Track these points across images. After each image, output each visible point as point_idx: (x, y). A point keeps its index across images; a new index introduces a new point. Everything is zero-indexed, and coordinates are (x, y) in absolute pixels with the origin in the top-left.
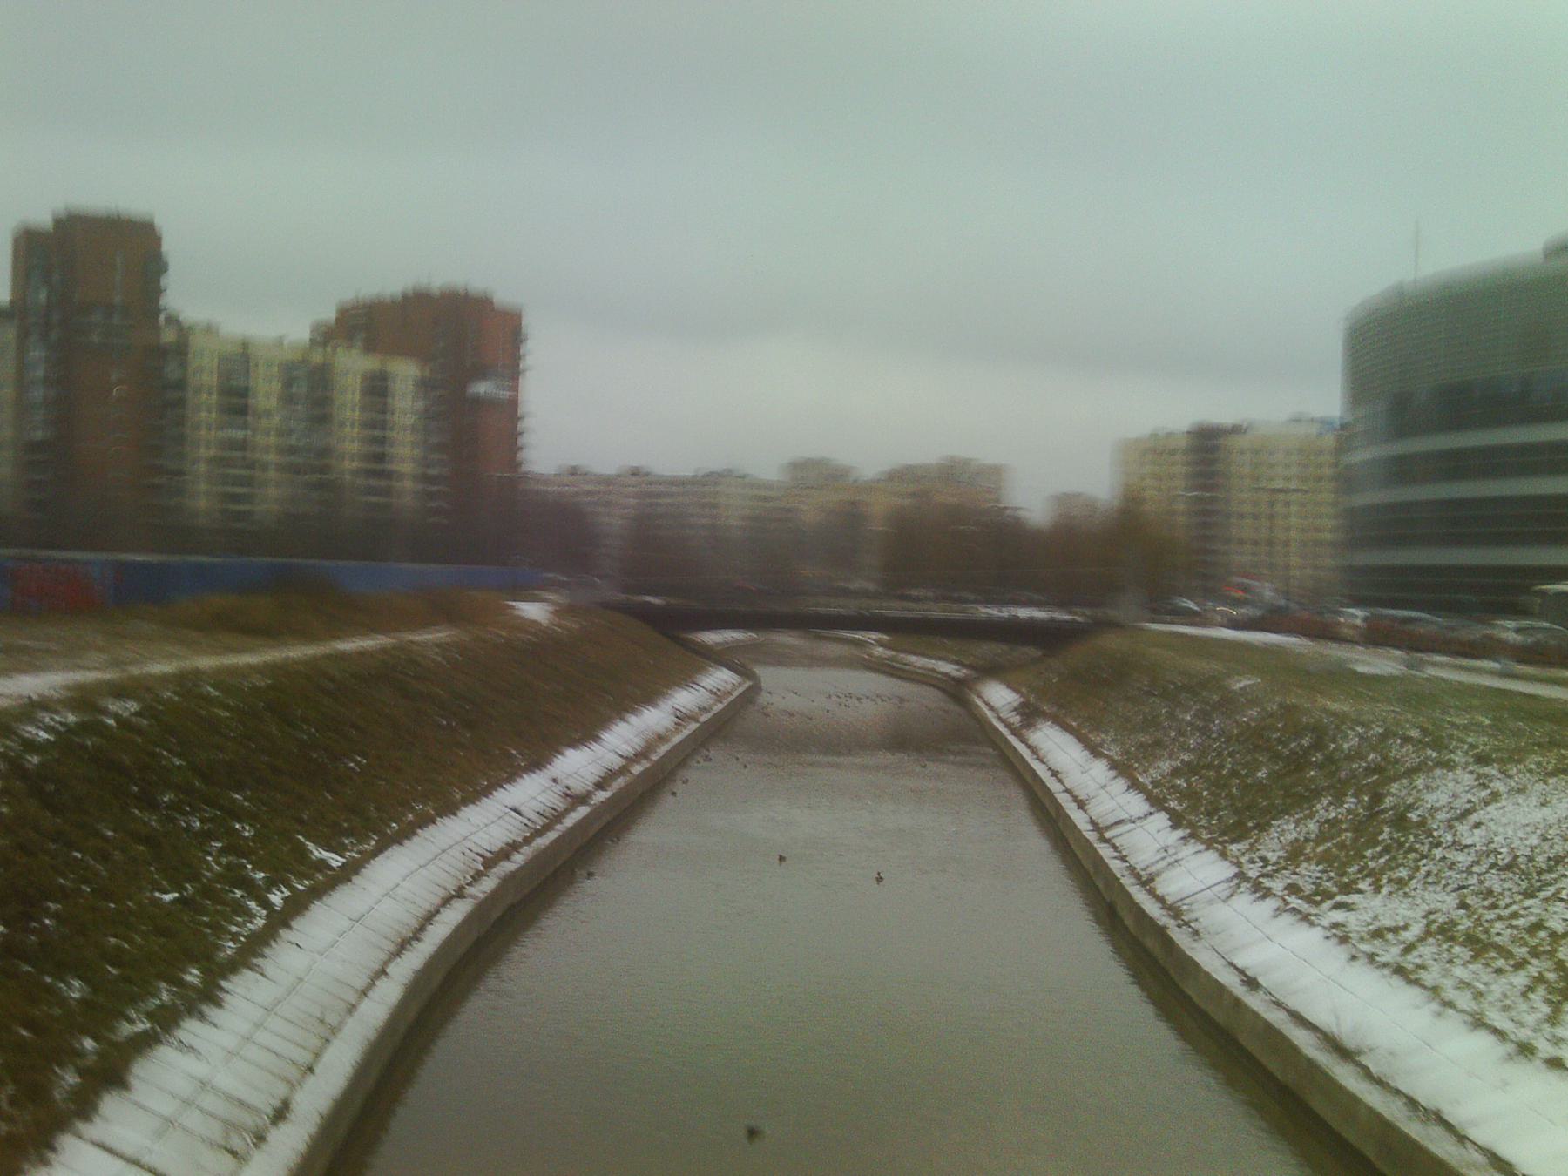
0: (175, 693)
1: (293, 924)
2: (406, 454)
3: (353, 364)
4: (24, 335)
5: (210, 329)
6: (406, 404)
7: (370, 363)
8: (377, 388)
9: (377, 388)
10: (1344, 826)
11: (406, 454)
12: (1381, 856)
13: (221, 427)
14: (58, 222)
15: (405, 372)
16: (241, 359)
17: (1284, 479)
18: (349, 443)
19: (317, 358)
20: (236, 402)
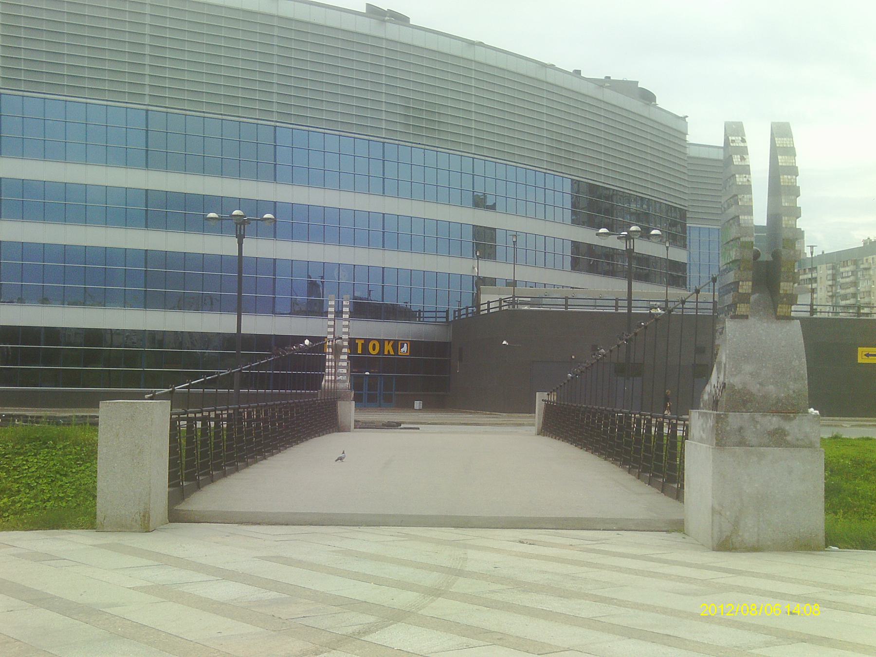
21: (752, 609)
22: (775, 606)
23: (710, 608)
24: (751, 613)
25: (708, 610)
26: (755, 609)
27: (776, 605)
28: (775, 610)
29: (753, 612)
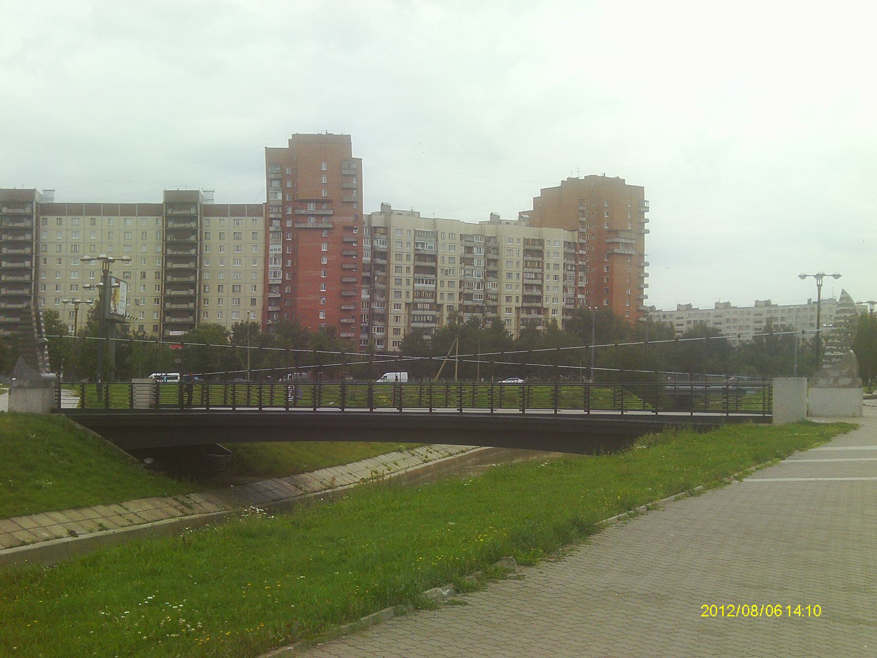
4: (269, 222)
21: (753, 610)
22: (776, 607)
23: (711, 609)
24: (752, 614)
25: (709, 611)
26: (756, 610)
27: (777, 606)
28: (775, 611)
29: (755, 613)
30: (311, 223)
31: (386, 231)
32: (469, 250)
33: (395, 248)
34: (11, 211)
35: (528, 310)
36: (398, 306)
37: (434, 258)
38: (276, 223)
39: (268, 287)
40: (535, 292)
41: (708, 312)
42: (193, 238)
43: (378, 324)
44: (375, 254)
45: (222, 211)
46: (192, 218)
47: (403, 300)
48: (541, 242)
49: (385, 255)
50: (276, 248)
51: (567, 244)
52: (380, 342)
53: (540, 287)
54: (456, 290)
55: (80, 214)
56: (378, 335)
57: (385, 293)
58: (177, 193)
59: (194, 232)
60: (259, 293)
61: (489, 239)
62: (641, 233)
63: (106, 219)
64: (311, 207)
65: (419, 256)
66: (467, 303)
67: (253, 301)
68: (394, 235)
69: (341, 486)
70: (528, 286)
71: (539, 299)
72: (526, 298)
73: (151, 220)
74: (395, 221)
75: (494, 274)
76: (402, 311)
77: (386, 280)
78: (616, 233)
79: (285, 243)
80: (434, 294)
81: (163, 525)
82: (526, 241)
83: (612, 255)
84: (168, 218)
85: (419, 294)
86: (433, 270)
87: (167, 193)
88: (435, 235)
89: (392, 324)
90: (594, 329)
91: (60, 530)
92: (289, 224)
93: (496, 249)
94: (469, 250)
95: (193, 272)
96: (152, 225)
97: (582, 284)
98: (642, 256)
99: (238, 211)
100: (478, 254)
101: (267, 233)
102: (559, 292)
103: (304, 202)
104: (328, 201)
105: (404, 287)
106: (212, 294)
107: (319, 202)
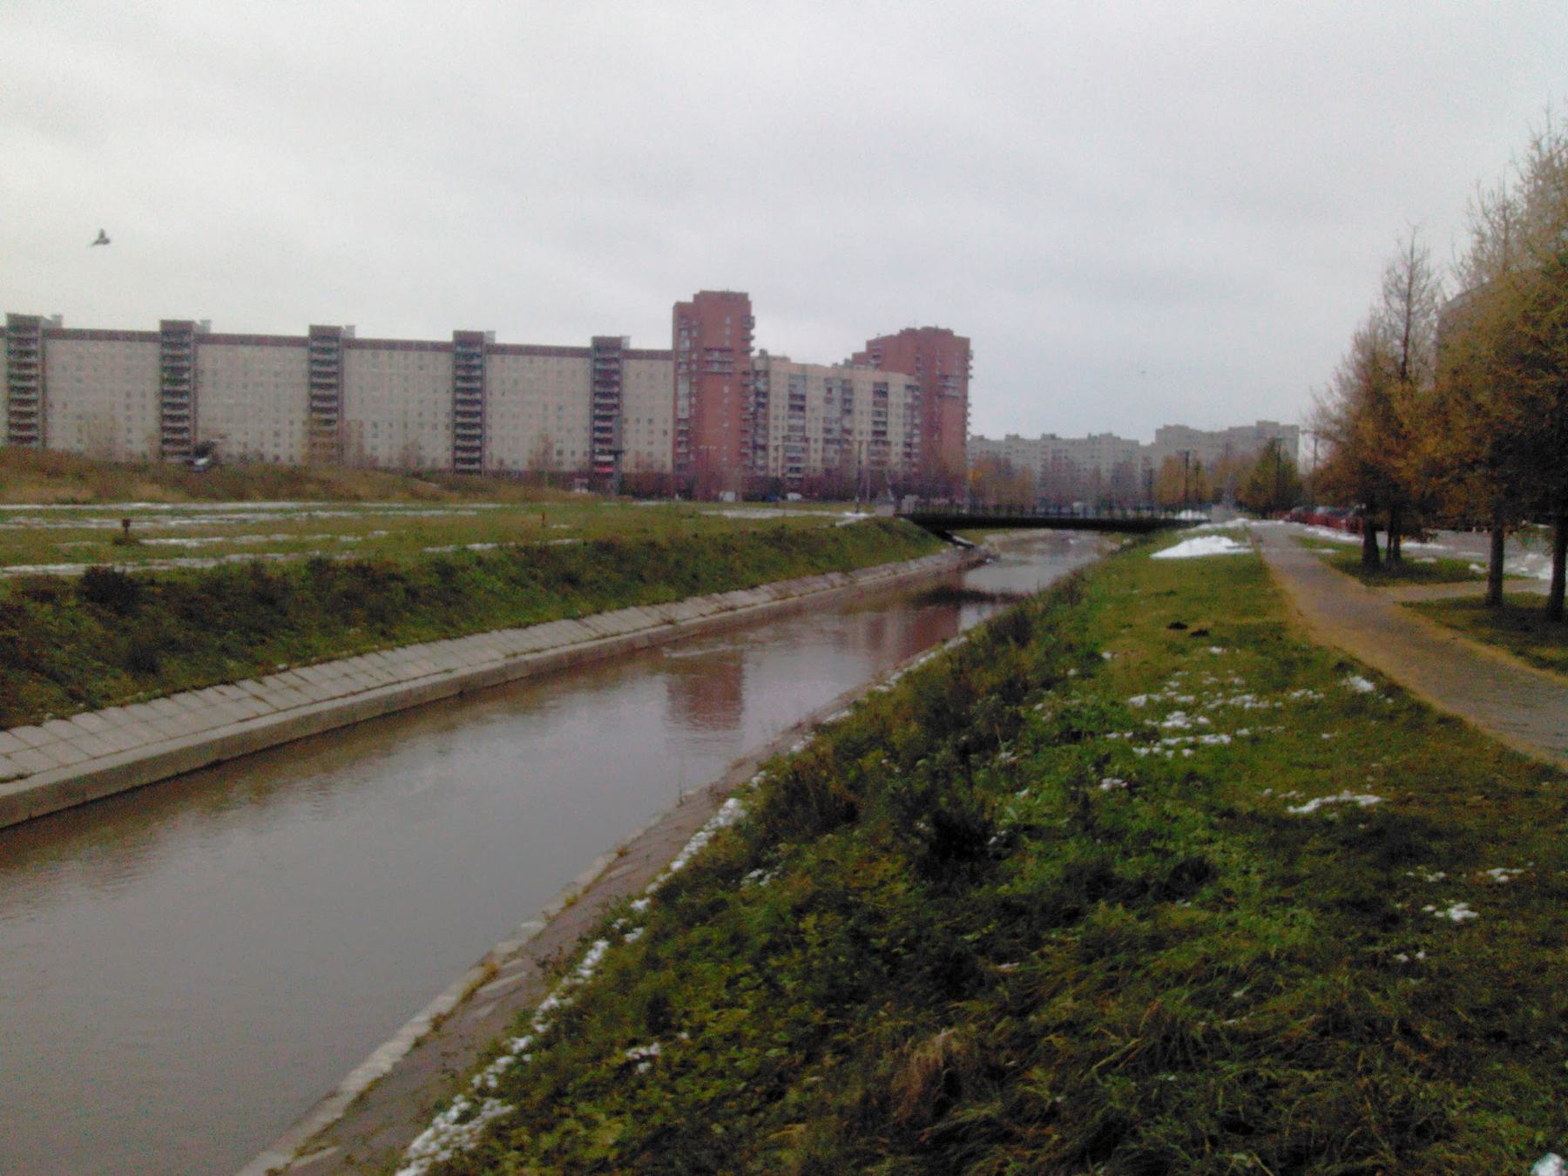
0: (887, 495)
1: (1086, 436)
2: (897, 433)
3: (867, 378)
4: (678, 365)
5: (785, 359)
6: (898, 397)
7: (879, 376)
8: (881, 392)
9: (881, 392)
10: (1382, 539)
11: (897, 433)
12: (1504, 932)
13: (790, 417)
14: (696, 297)
15: (898, 382)
16: (804, 373)
17: (1347, 715)
18: (862, 425)
19: (846, 374)
20: (798, 404)
30: (716, 368)
31: (767, 374)
32: (830, 390)
33: (774, 389)
34: (464, 350)
35: (876, 442)
36: (776, 438)
37: (803, 397)
38: (684, 367)
39: (678, 421)
40: (881, 428)
41: (997, 443)
42: (166, 376)
43: (760, 453)
44: (758, 393)
45: (504, 350)
46: (616, 360)
47: (780, 433)
48: (886, 384)
49: (765, 395)
50: (684, 388)
51: (908, 387)
52: (762, 468)
53: (885, 423)
54: (821, 425)
55: (536, 354)
56: (760, 462)
57: (766, 427)
58: (23, 318)
59: (617, 372)
60: (670, 426)
61: (844, 382)
62: (965, 378)
63: (542, 358)
64: (716, 355)
65: (793, 396)
66: (829, 436)
67: (665, 433)
68: (773, 378)
69: (553, 647)
70: (876, 423)
71: (884, 433)
72: (876, 433)
73: (579, 361)
74: (775, 368)
75: (849, 412)
76: (779, 442)
77: (766, 416)
78: (946, 377)
79: (691, 384)
80: (803, 429)
81: (367, 702)
82: (876, 384)
83: (941, 396)
84: (457, 355)
85: (792, 428)
86: (802, 408)
87: (164, 323)
88: (805, 378)
89: (772, 453)
90: (499, 506)
91: (494, 654)
92: (694, 367)
93: (851, 391)
94: (830, 390)
95: (479, 414)
96: (583, 367)
97: (917, 421)
98: (966, 397)
99: (652, 355)
100: (836, 393)
101: (676, 374)
102: (900, 429)
103: (709, 350)
104: (730, 350)
105: (780, 423)
106: (630, 428)
107: (722, 350)
